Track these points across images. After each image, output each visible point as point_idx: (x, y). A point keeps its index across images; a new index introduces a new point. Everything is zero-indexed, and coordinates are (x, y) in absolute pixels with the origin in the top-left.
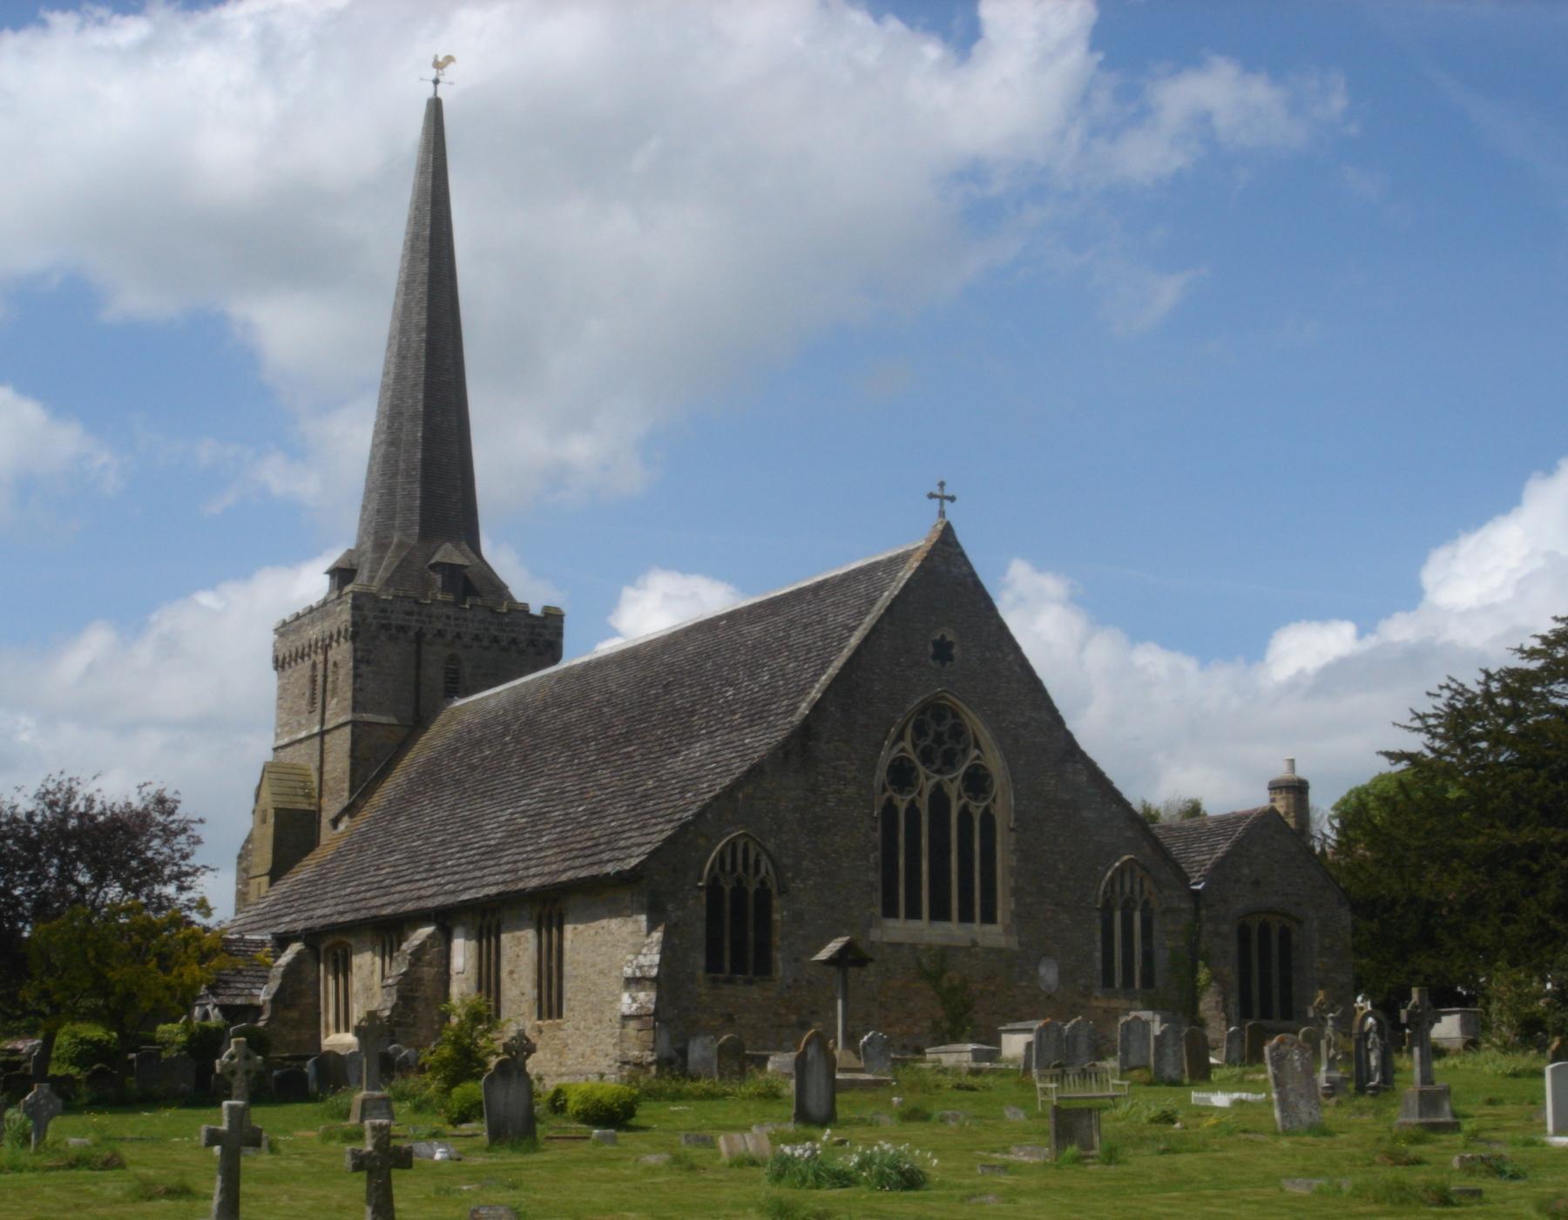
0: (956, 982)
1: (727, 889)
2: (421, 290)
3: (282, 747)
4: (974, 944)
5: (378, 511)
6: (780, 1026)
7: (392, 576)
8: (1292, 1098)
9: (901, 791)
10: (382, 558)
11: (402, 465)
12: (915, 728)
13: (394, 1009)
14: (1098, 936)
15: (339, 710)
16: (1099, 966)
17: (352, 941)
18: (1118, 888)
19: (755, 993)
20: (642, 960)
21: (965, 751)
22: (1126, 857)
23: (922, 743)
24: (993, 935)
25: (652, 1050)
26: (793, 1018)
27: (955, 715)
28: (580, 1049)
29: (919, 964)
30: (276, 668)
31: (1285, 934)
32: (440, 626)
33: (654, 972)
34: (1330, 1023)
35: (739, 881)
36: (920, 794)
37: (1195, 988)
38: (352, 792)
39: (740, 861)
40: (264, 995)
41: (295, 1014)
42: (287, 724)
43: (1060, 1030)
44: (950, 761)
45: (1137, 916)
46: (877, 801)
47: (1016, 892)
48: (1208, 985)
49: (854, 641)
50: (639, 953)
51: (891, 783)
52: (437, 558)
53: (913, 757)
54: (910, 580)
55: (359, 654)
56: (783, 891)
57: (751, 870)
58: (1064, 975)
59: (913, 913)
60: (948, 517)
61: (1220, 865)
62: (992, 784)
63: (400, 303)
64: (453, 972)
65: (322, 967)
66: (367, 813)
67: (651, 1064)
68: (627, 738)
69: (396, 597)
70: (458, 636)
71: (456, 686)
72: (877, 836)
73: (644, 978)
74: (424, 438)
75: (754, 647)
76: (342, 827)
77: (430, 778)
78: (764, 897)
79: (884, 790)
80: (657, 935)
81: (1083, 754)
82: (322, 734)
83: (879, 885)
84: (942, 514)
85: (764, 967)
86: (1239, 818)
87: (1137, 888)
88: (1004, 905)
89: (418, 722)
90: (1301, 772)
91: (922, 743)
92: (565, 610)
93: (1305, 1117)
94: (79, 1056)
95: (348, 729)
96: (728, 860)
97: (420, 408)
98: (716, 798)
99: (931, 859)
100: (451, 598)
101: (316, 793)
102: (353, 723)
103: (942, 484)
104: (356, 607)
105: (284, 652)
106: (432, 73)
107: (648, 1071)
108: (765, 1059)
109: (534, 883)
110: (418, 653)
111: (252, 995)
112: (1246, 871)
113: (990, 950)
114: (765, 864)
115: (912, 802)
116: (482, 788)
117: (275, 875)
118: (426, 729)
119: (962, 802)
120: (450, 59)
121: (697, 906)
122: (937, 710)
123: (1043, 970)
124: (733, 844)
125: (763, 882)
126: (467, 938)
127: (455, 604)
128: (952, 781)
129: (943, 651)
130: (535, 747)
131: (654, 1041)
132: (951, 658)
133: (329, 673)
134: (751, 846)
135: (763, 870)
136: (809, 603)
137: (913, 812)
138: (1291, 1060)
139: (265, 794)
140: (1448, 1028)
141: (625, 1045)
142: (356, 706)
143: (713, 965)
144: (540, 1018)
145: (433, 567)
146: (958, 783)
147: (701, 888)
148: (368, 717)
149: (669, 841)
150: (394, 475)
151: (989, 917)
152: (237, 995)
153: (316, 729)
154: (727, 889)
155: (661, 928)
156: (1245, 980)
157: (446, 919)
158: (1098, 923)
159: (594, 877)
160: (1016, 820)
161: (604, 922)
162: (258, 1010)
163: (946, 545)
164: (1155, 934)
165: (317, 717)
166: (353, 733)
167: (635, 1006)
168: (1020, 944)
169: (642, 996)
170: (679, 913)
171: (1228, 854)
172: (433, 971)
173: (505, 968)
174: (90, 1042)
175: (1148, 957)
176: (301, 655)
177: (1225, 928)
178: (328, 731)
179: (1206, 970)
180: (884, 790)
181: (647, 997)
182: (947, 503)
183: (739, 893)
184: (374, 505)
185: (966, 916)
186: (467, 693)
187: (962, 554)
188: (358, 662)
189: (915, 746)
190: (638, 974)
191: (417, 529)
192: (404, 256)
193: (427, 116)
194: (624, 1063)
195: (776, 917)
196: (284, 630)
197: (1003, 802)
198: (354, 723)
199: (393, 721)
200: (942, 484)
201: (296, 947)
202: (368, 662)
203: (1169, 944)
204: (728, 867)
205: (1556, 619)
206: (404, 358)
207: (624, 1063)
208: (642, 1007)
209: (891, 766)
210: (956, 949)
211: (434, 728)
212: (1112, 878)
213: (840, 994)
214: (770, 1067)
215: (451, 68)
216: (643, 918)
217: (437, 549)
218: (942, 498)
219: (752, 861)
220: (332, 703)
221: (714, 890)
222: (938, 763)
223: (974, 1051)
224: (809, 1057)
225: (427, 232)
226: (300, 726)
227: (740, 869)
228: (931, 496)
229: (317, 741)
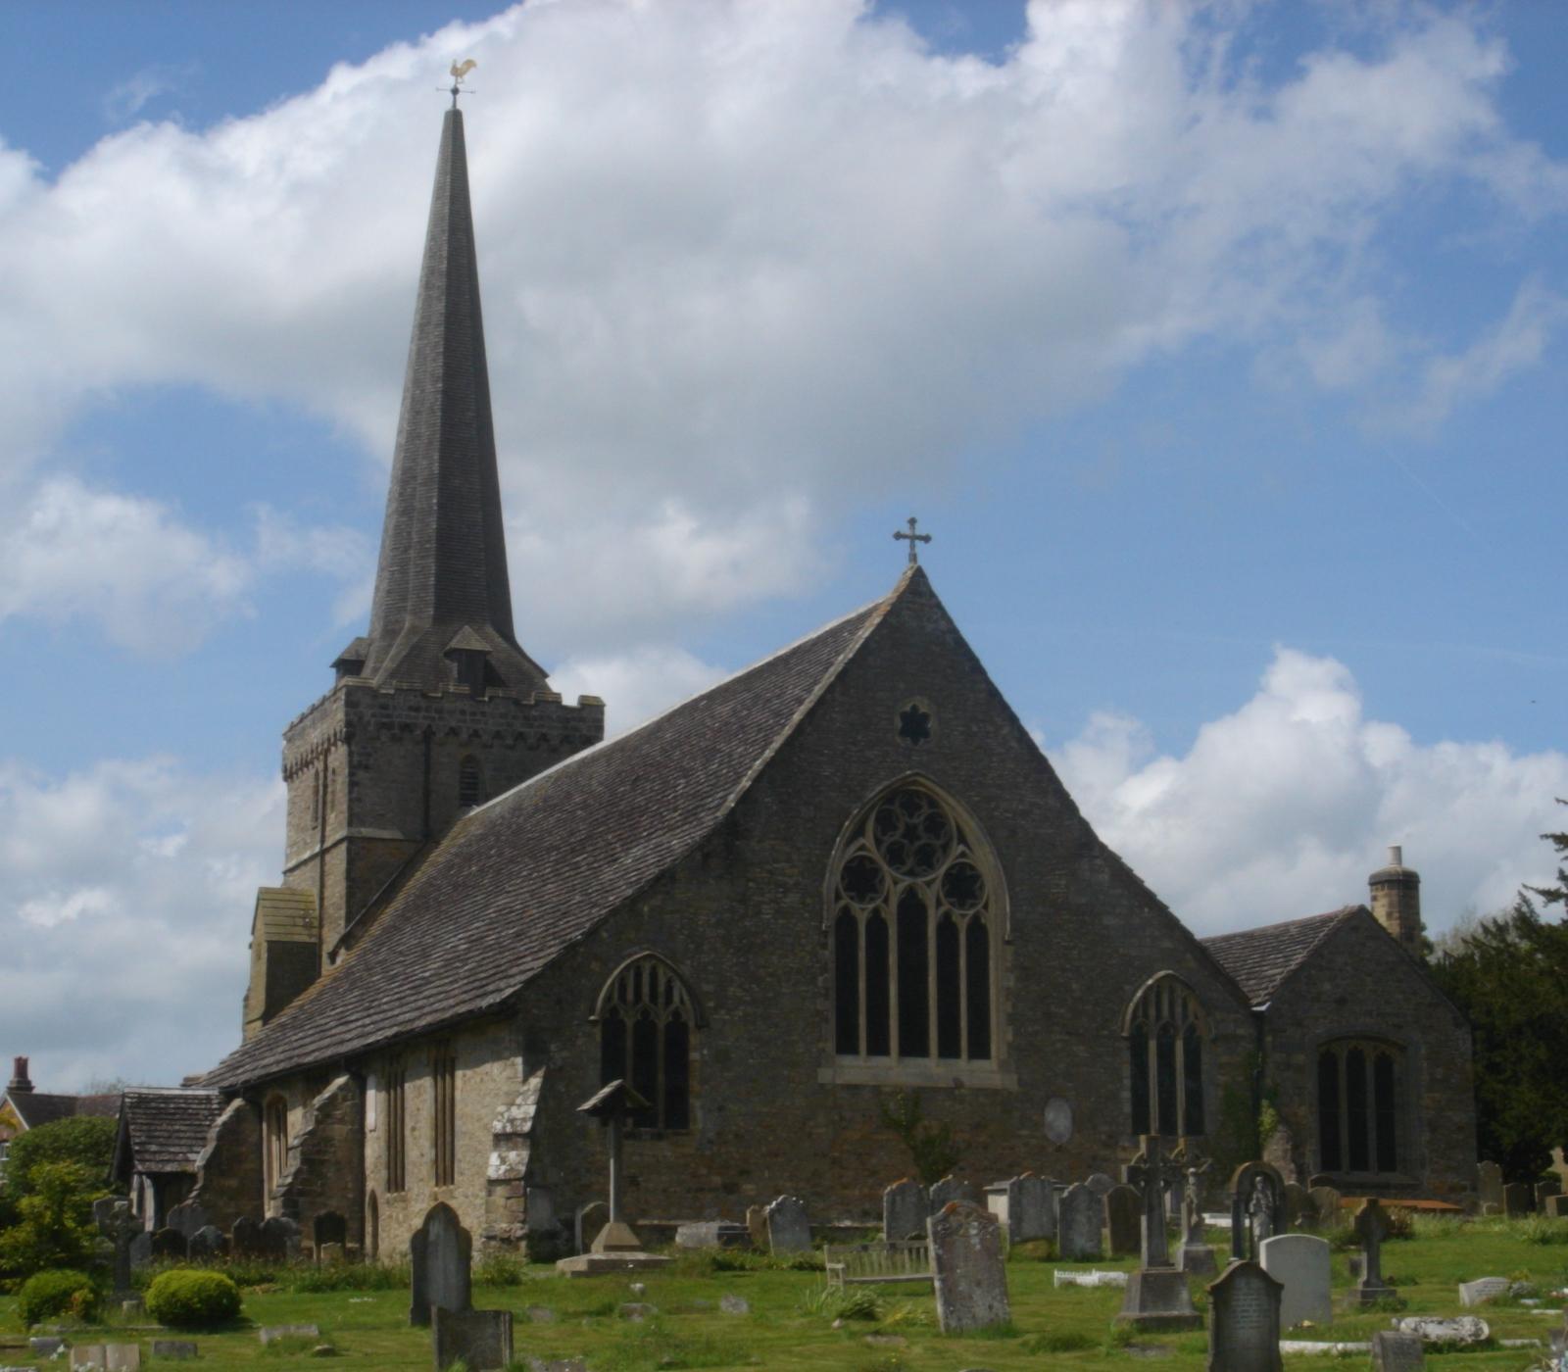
0: (935, 1132)
1: (629, 1023)
2: (437, 334)
4: (959, 1084)
5: (389, 592)
6: (701, 1190)
7: (399, 666)
8: (963, 1287)
9: (861, 899)
10: (390, 646)
11: (415, 538)
12: (878, 820)
14: (1127, 1071)
15: (337, 827)
16: (1127, 1108)
17: (286, 1095)
18: (1152, 1012)
19: (665, 1150)
20: (515, 1112)
21: (946, 848)
22: (1162, 973)
23: (888, 840)
25: (523, 1222)
26: (717, 1180)
27: (933, 803)
31: (1384, 1065)
32: (453, 724)
33: (527, 1127)
34: (1191, 1180)
35: (645, 1013)
36: (886, 901)
37: (1257, 1134)
38: (348, 920)
39: (646, 990)
40: (199, 1159)
41: (233, 1183)
44: (926, 859)
45: (1179, 1046)
47: (1012, 1019)
48: (1273, 1129)
49: (797, 717)
50: (512, 1104)
51: (947, 895)
52: (454, 644)
53: (875, 854)
54: (868, 640)
56: (703, 1025)
57: (661, 1000)
58: (1077, 1123)
59: (878, 1047)
60: (921, 562)
61: (1292, 978)
62: (982, 887)
63: (414, 348)
64: (367, 1130)
65: (265, 1126)
66: (364, 943)
67: (519, 1239)
70: (476, 734)
71: (473, 794)
72: (828, 954)
74: (441, 505)
76: (339, 961)
79: (838, 897)
80: (535, 1082)
81: (1103, 848)
82: (323, 852)
84: (913, 557)
85: (678, 1117)
86: (1325, 921)
87: (1179, 1010)
88: (1000, 1036)
89: (429, 837)
90: (1409, 864)
91: (888, 840)
92: (605, 699)
93: (981, 1312)
95: (344, 847)
97: (436, 468)
99: (903, 979)
100: (466, 689)
101: (316, 923)
103: (912, 522)
106: (450, 81)
107: (517, 1248)
108: (674, 1229)
111: (187, 1160)
112: (1327, 986)
113: (978, 1092)
115: (876, 911)
117: (266, 1017)
118: (438, 843)
119: (942, 910)
122: (906, 798)
124: (637, 968)
125: (676, 1014)
126: (378, 1089)
127: (472, 697)
128: (929, 884)
129: (915, 726)
130: (512, 861)
131: (525, 1211)
132: (926, 734)
134: (661, 971)
135: (676, 999)
137: (877, 924)
138: (967, 1236)
139: (259, 925)
141: (493, 1216)
142: (353, 819)
144: (437, 1185)
145: (452, 654)
146: (937, 885)
147: (594, 1023)
148: (366, 832)
149: (552, 966)
150: (406, 550)
151: (979, 1050)
152: (168, 1161)
153: (317, 849)
154: (629, 1023)
155: (541, 1073)
157: (360, 1065)
158: (1126, 1055)
159: (470, 1012)
160: (1013, 930)
161: (487, 1067)
162: (193, 1177)
163: (917, 592)
164: (1205, 1067)
166: (349, 851)
168: (1020, 1082)
169: (512, 1155)
170: (565, 1054)
171: (1302, 966)
173: (409, 1123)
175: (1195, 1098)
177: (1299, 1058)
179: (1271, 1111)
181: (517, 1158)
182: (918, 543)
184: (385, 586)
185: (949, 1050)
187: (939, 606)
188: (354, 768)
189: (878, 842)
190: (509, 1129)
192: (419, 295)
195: (694, 1056)
196: (293, 733)
197: (998, 911)
198: (349, 839)
199: (398, 835)
200: (912, 522)
201: (237, 1102)
202: (367, 768)
204: (630, 996)
206: (418, 413)
207: (490, 1238)
208: (511, 1169)
209: (847, 869)
210: (936, 1090)
211: (445, 843)
212: (1145, 997)
213: (612, 1152)
214: (678, 1239)
216: (519, 1060)
217: (456, 633)
218: (914, 538)
219: (662, 988)
220: (332, 817)
221: (612, 1025)
222: (910, 863)
224: (432, 1237)
225: (444, 266)
227: (646, 998)
228: (898, 536)
229: (317, 861)
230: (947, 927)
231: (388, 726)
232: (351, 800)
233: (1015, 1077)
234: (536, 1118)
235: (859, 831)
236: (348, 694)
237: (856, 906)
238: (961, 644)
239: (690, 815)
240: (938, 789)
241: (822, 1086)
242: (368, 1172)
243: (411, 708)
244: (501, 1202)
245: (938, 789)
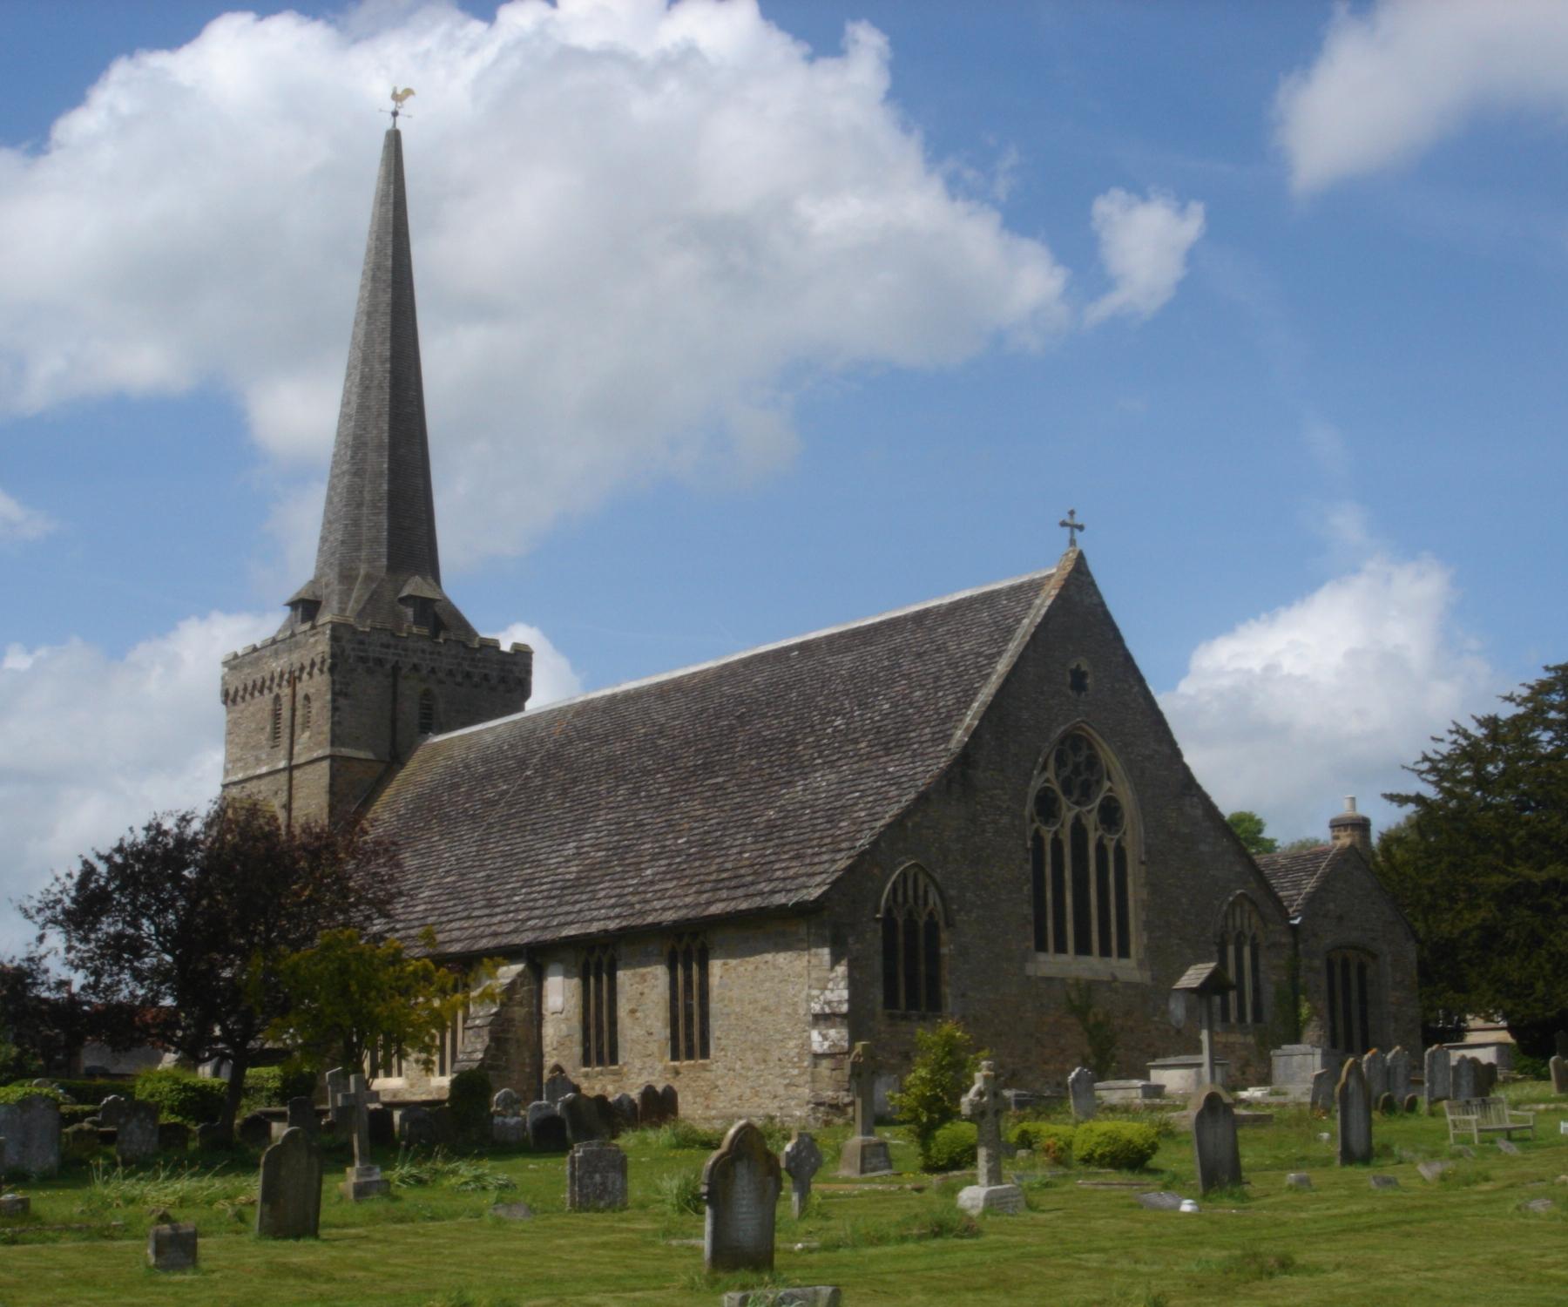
0: (1101, 1017)
3: (235, 783)
4: (1115, 979)
5: (343, 542)
9: (1046, 823)
10: (351, 590)
11: (367, 496)
13: (487, 1051)
15: (312, 743)
20: (829, 995)
21: (1099, 782)
27: (1091, 747)
28: (735, 1092)
29: (1070, 1000)
30: (225, 702)
31: (1362, 968)
32: (415, 660)
35: (910, 913)
39: (910, 893)
42: (239, 760)
43: (1384, 1060)
44: (1086, 794)
45: (1247, 951)
46: (998, 830)
49: (1002, 666)
50: (825, 988)
52: (404, 594)
53: (1056, 787)
54: (1050, 607)
55: (338, 687)
56: (950, 924)
57: (921, 902)
59: (1061, 948)
61: (1312, 899)
62: (1122, 817)
64: (546, 1012)
68: (708, 768)
69: (373, 628)
71: (430, 724)
72: (1029, 867)
73: (834, 1015)
74: (390, 469)
75: (852, 677)
78: (932, 928)
80: (841, 969)
81: (1198, 788)
83: (1032, 918)
84: (1072, 542)
89: (395, 759)
94: (182, 1103)
95: (326, 764)
96: (900, 892)
97: (386, 438)
98: (888, 826)
100: (425, 631)
102: (332, 757)
104: (335, 638)
105: (235, 683)
106: (391, 106)
109: (670, 916)
110: (394, 685)
112: (1331, 906)
113: (1128, 985)
114: (933, 897)
116: (514, 823)
118: (403, 765)
120: (409, 92)
121: (874, 937)
122: (1075, 740)
123: (1172, 1006)
124: (904, 874)
125: (931, 915)
128: (1089, 812)
133: (299, 705)
134: (921, 877)
135: (931, 902)
136: (913, 632)
137: (1057, 844)
141: (818, 1085)
142: (335, 740)
143: (890, 1001)
144: (675, 1057)
145: (403, 601)
147: (878, 920)
148: (346, 751)
149: (849, 870)
150: (359, 505)
151: (1124, 952)
153: (282, 764)
155: (844, 962)
156: (1332, 1010)
157: (538, 958)
160: (1147, 852)
161: (769, 957)
163: (1079, 577)
165: (282, 752)
166: (331, 767)
167: (826, 1044)
169: (832, 1033)
170: (858, 946)
172: (524, 1010)
174: (193, 1089)
176: (260, 688)
178: (298, 766)
180: (1033, 821)
182: (1076, 531)
183: (911, 922)
186: (441, 730)
187: (1093, 584)
189: (1057, 776)
190: (827, 1010)
191: (384, 561)
193: (387, 147)
194: (819, 1104)
195: (944, 950)
196: (234, 663)
197: (1133, 834)
199: (370, 756)
200: (1072, 513)
202: (346, 695)
203: (1274, 978)
204: (900, 899)
205: (1547, 669)
207: (819, 1104)
208: (834, 1045)
211: (412, 765)
215: (409, 101)
216: (825, 952)
217: (405, 582)
219: (921, 892)
220: (304, 738)
221: (889, 923)
223: (1143, 1087)
225: (389, 263)
226: (258, 761)
227: (911, 900)
229: (283, 777)
231: (363, 660)
232: (333, 723)
233: (1149, 973)
234: (850, 1001)
235: (1044, 768)
236: (333, 630)
237: (1044, 829)
238: (1107, 616)
239: (891, 741)
240: (1095, 735)
241: (1028, 977)
242: (547, 1049)
243: (382, 645)
244: (827, 1073)
245: (1095, 735)
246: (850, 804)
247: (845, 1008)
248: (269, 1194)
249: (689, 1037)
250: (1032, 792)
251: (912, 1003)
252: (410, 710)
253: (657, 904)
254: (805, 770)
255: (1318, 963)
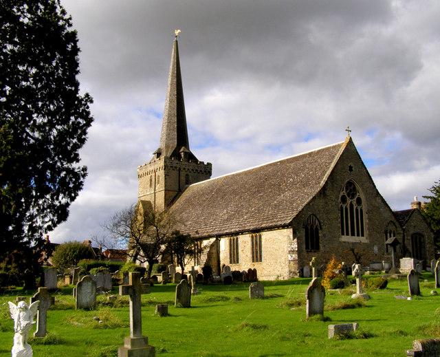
15: (161, 187)
21: (356, 193)
24: (364, 240)
31: (420, 239)
44: (353, 197)
47: (369, 229)
49: (333, 165)
56: (321, 228)
59: (347, 234)
68: (259, 192)
71: (188, 182)
77: (188, 201)
80: (296, 240)
89: (180, 191)
95: (163, 192)
99: (351, 223)
122: (350, 184)
140: (407, 264)
151: (363, 235)
177: (409, 238)
197: (364, 206)
220: (158, 186)
230: (357, 210)
231: (172, 167)
234: (298, 248)
246: (299, 198)
247: (297, 249)
248: (178, 297)
249: (257, 257)
250: (340, 196)
251: (312, 248)
252: (183, 178)
253: (248, 225)
254: (284, 191)
255: (409, 238)
